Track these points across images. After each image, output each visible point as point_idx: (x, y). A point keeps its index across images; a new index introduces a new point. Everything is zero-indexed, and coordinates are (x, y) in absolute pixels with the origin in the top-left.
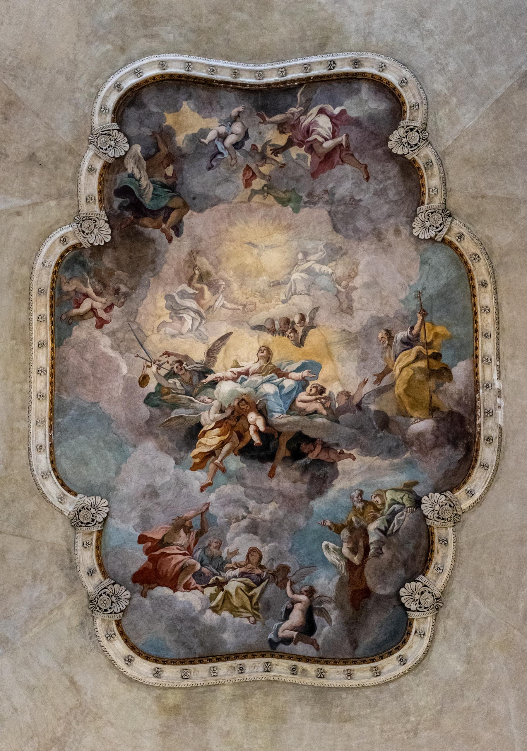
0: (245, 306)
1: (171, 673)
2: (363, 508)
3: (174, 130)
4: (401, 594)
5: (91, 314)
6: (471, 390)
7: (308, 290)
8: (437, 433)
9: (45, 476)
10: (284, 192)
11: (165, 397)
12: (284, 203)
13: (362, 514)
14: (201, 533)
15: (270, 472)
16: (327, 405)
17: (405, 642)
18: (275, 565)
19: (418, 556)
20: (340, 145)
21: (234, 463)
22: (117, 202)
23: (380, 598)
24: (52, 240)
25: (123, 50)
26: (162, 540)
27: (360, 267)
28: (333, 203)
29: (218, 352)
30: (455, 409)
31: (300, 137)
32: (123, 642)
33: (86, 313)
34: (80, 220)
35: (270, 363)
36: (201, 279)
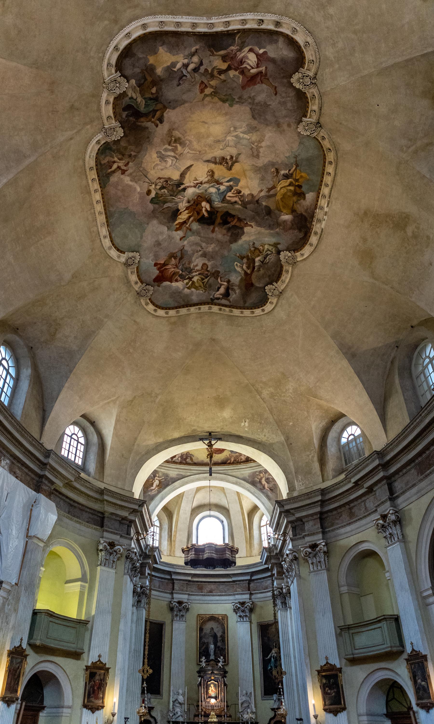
0: (200, 152)
1: (172, 313)
2: (254, 250)
3: (155, 66)
4: (266, 288)
5: (118, 169)
6: (313, 207)
7: (236, 145)
8: (293, 222)
9: (110, 248)
10: (224, 96)
11: (161, 199)
12: (224, 101)
13: (253, 253)
14: (181, 258)
15: (212, 230)
16: (242, 199)
17: (265, 305)
18: (214, 271)
19: (276, 274)
20: (261, 72)
21: (195, 226)
22: (124, 114)
23: (257, 288)
24: (92, 145)
25: (116, 21)
26: (164, 263)
27: (266, 138)
28: (253, 104)
29: (186, 174)
30: (304, 213)
31: (236, 65)
32: (152, 305)
33: (115, 170)
34: (106, 132)
35: (214, 178)
36: (175, 141)
